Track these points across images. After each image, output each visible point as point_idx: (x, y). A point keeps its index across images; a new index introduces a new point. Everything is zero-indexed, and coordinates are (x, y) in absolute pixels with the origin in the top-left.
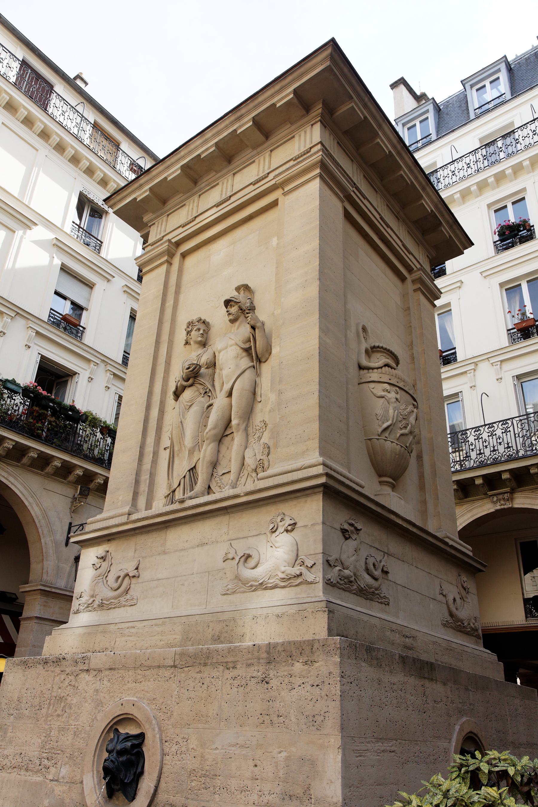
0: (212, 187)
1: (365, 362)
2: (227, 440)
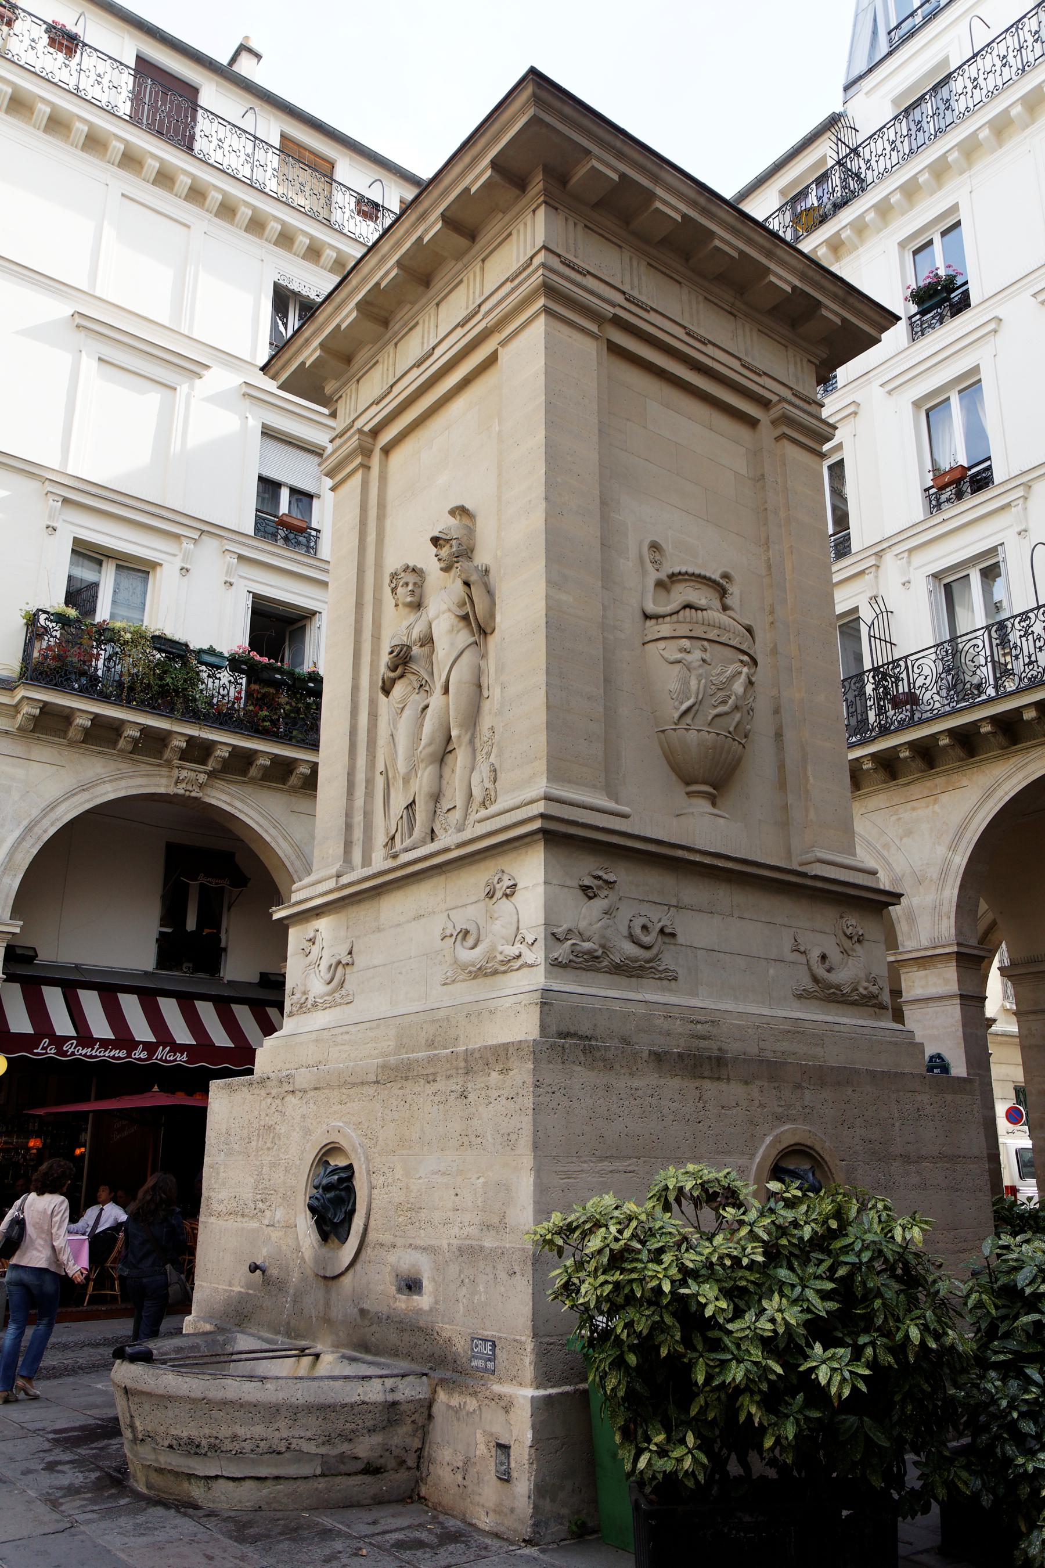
0: (411, 329)
1: (651, 608)
2: (450, 758)
